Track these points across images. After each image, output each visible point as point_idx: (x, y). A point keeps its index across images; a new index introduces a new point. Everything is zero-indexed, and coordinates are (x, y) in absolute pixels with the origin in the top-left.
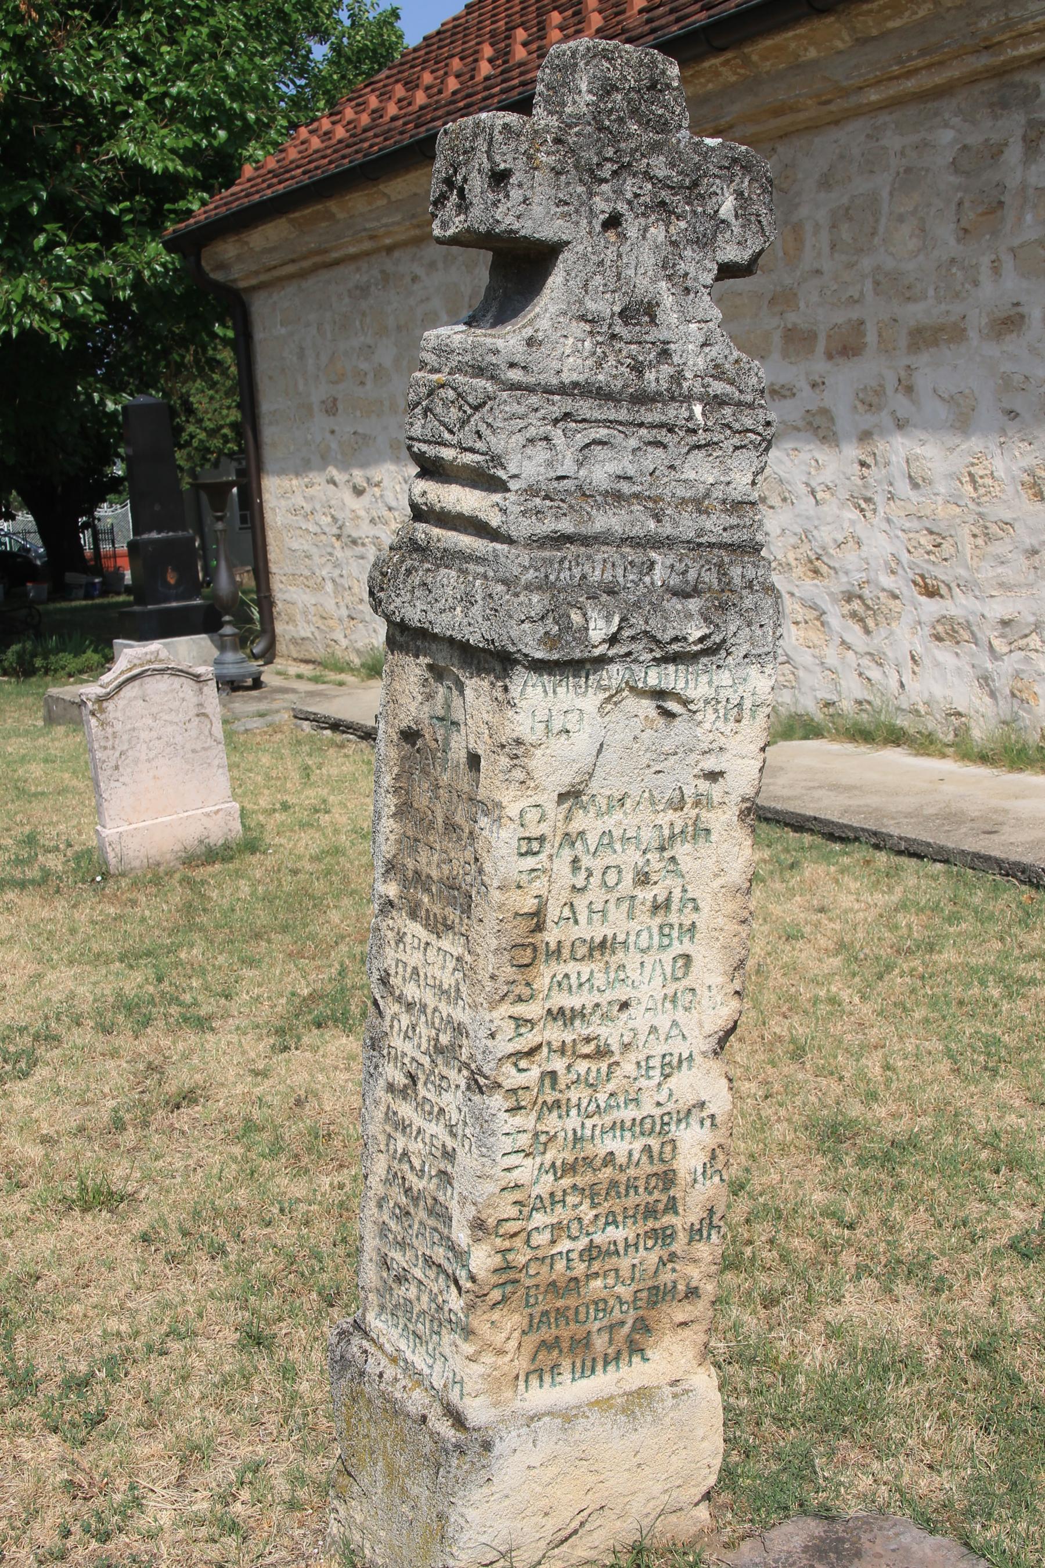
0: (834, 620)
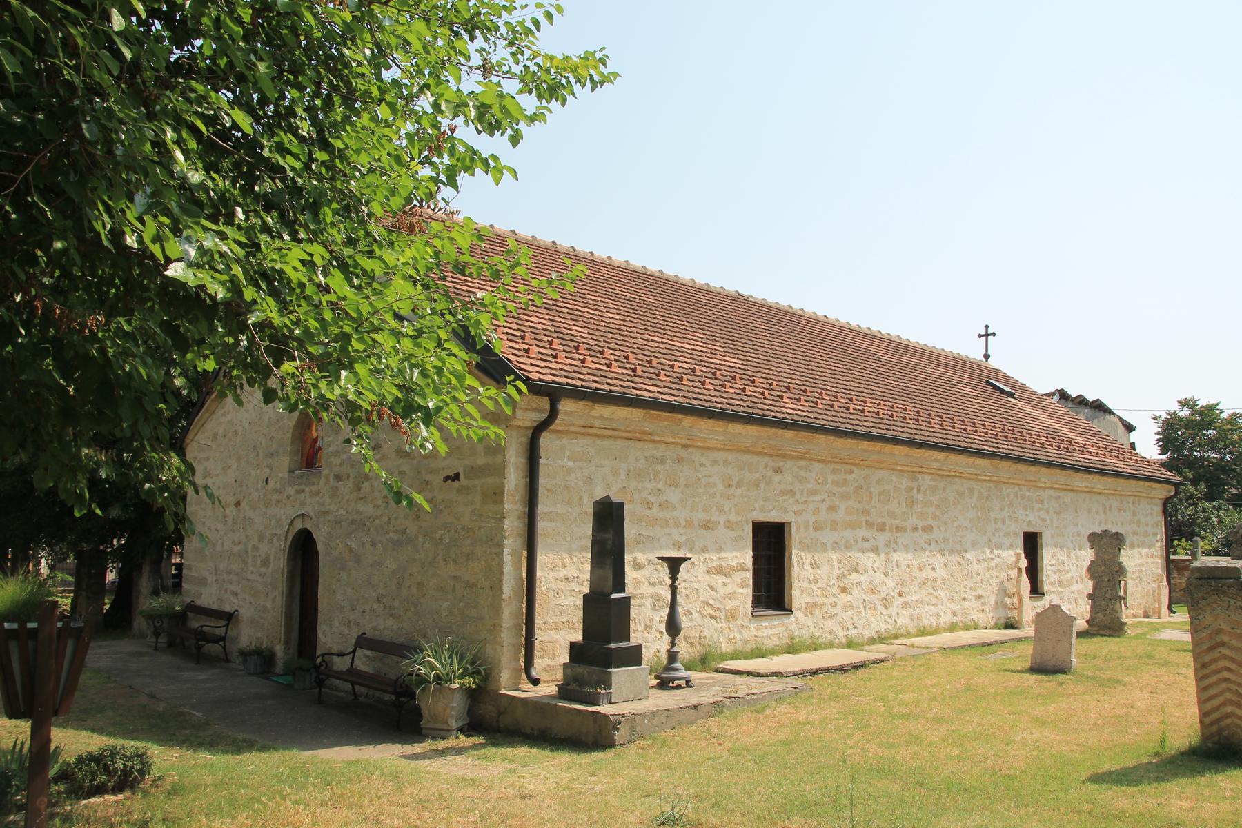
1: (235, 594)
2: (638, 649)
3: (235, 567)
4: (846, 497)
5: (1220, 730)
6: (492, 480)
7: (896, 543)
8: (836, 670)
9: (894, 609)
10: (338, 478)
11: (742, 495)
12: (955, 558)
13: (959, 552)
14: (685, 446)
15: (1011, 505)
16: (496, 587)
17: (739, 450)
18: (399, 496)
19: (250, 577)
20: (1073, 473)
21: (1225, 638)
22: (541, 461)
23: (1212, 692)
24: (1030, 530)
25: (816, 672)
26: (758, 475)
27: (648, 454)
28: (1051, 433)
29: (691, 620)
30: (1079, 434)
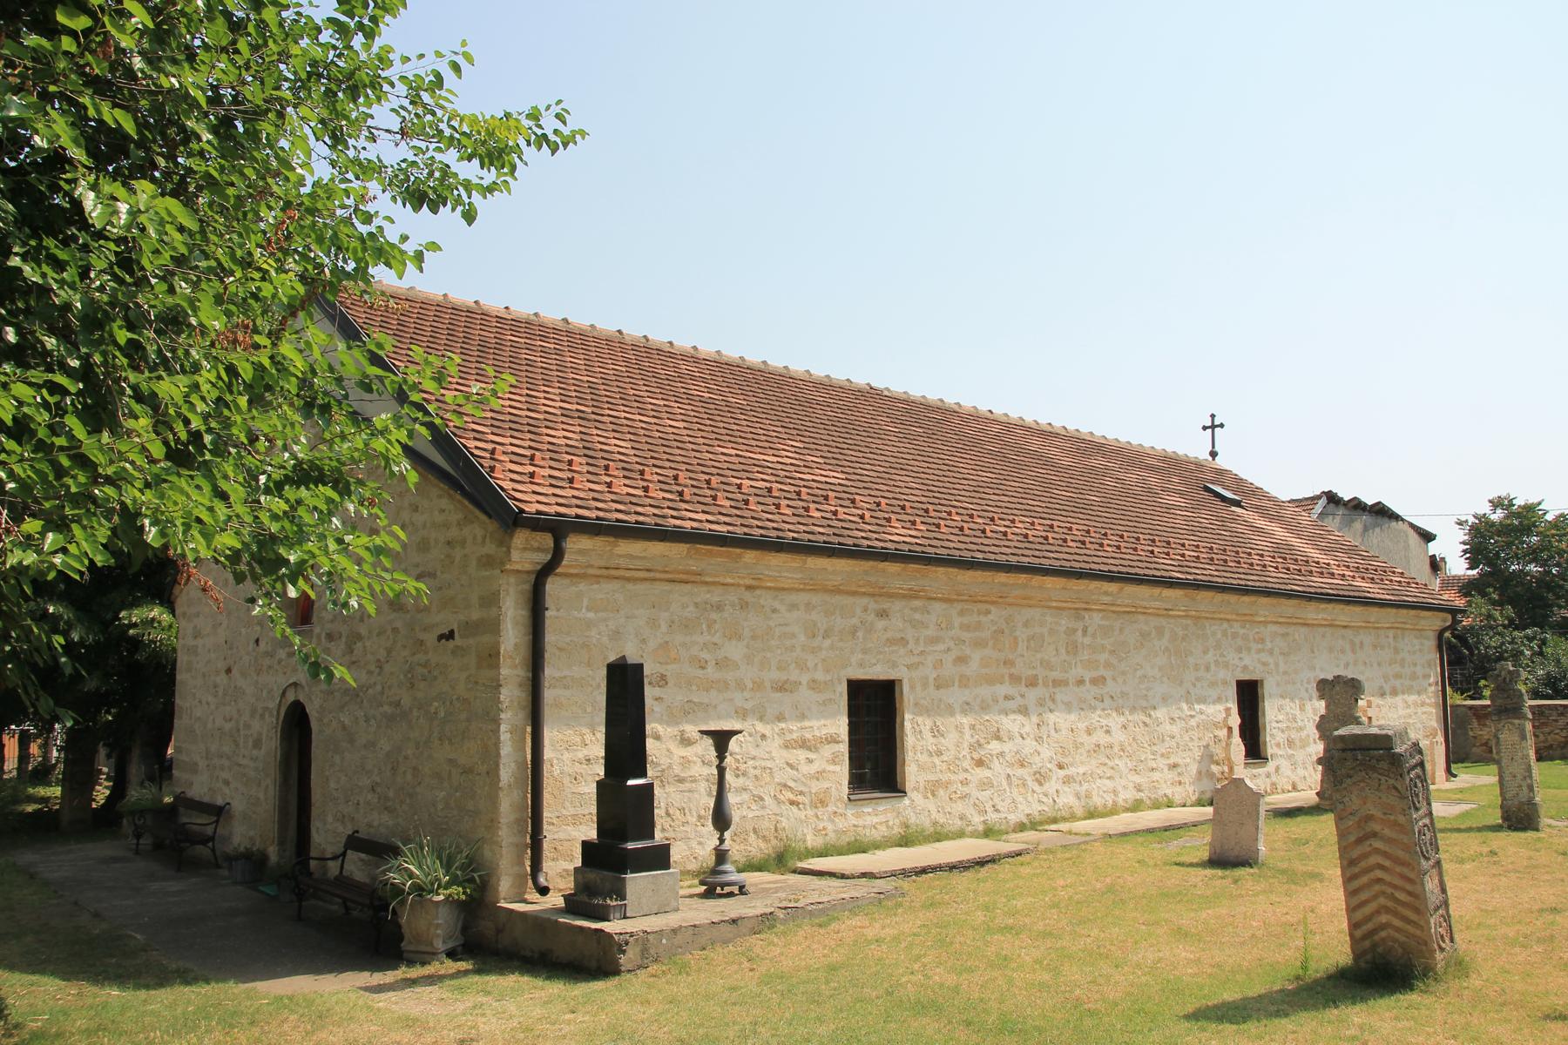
1: (227, 783)
3: (226, 749)
4: (979, 644)
5: (1374, 946)
7: (1053, 700)
8: (952, 867)
9: (1052, 786)
10: (330, 637)
11: (832, 647)
13: (1144, 709)
14: (749, 588)
15: (1218, 646)
16: (493, 773)
17: (826, 590)
20: (1304, 603)
21: (1377, 827)
22: (548, 614)
23: (1364, 896)
24: (1246, 677)
26: (855, 621)
28: (1283, 552)
29: (763, 807)
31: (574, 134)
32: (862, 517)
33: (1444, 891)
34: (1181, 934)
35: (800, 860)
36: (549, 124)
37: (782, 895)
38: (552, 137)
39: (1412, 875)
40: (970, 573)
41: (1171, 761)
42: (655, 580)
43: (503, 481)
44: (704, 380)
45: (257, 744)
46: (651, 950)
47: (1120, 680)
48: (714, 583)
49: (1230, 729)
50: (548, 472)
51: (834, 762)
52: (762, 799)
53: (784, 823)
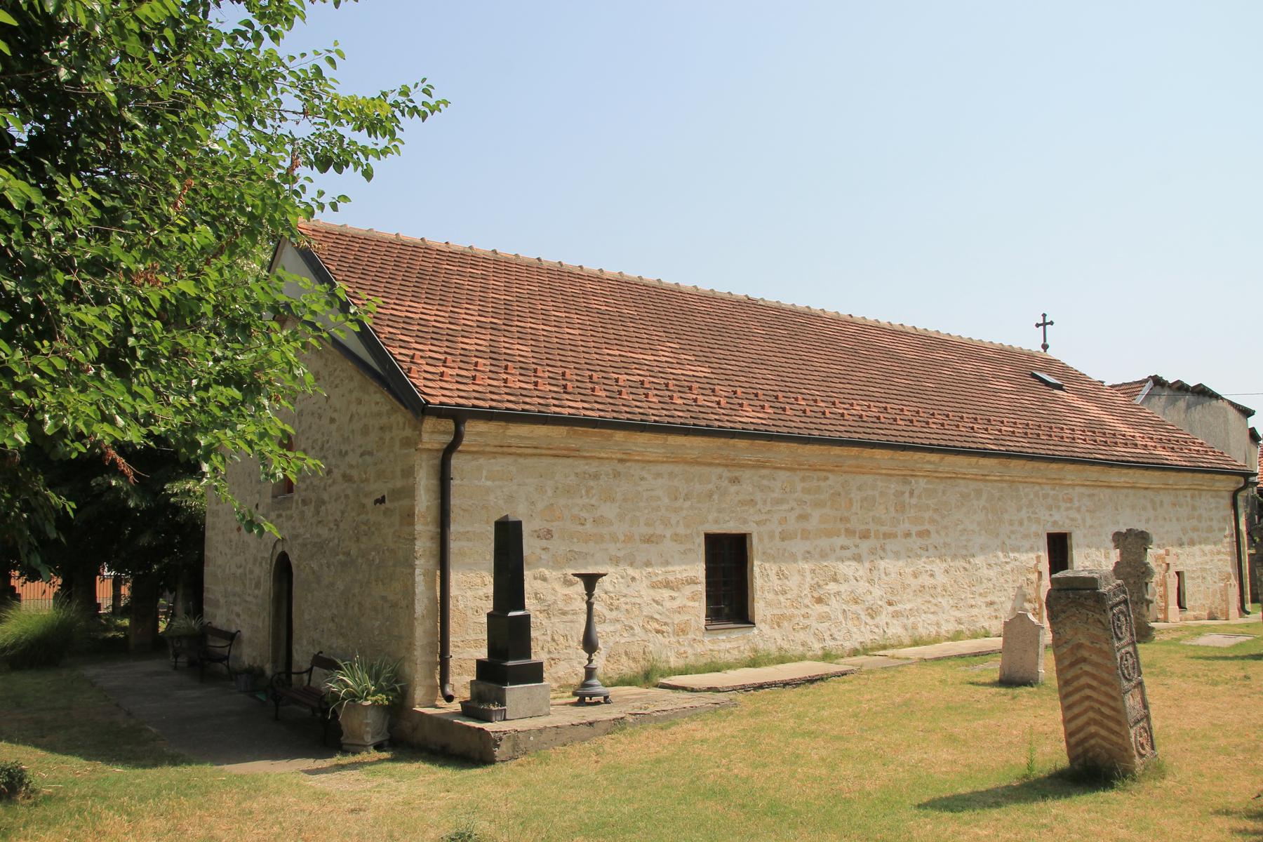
0: (863, 617)
1: (238, 615)
2: (539, 666)
3: (238, 589)
4: (819, 504)
5: (1086, 751)
6: (406, 502)
7: (884, 550)
8: (786, 684)
9: (882, 619)
11: (692, 508)
12: (960, 563)
13: (964, 557)
14: (621, 461)
15: (1030, 505)
16: (411, 606)
17: (686, 462)
18: (251, 524)
19: (248, 599)
20: (1107, 469)
21: (1086, 654)
23: (1076, 710)
25: (761, 687)
26: (710, 486)
27: (578, 470)
28: (1094, 427)
29: (633, 635)
30: (1132, 425)
31: (438, 103)
32: (719, 403)
33: (1145, 706)
34: (951, 739)
35: (662, 676)
36: (418, 98)
37: (638, 704)
38: (421, 108)
39: (1114, 694)
40: (808, 447)
41: (988, 599)
42: (541, 455)
43: (417, 380)
44: (604, 296)
45: (257, 586)
46: (520, 746)
47: (943, 533)
48: (591, 457)
49: (1040, 573)
50: (454, 372)
51: (693, 599)
52: (632, 628)
53: (651, 647)
